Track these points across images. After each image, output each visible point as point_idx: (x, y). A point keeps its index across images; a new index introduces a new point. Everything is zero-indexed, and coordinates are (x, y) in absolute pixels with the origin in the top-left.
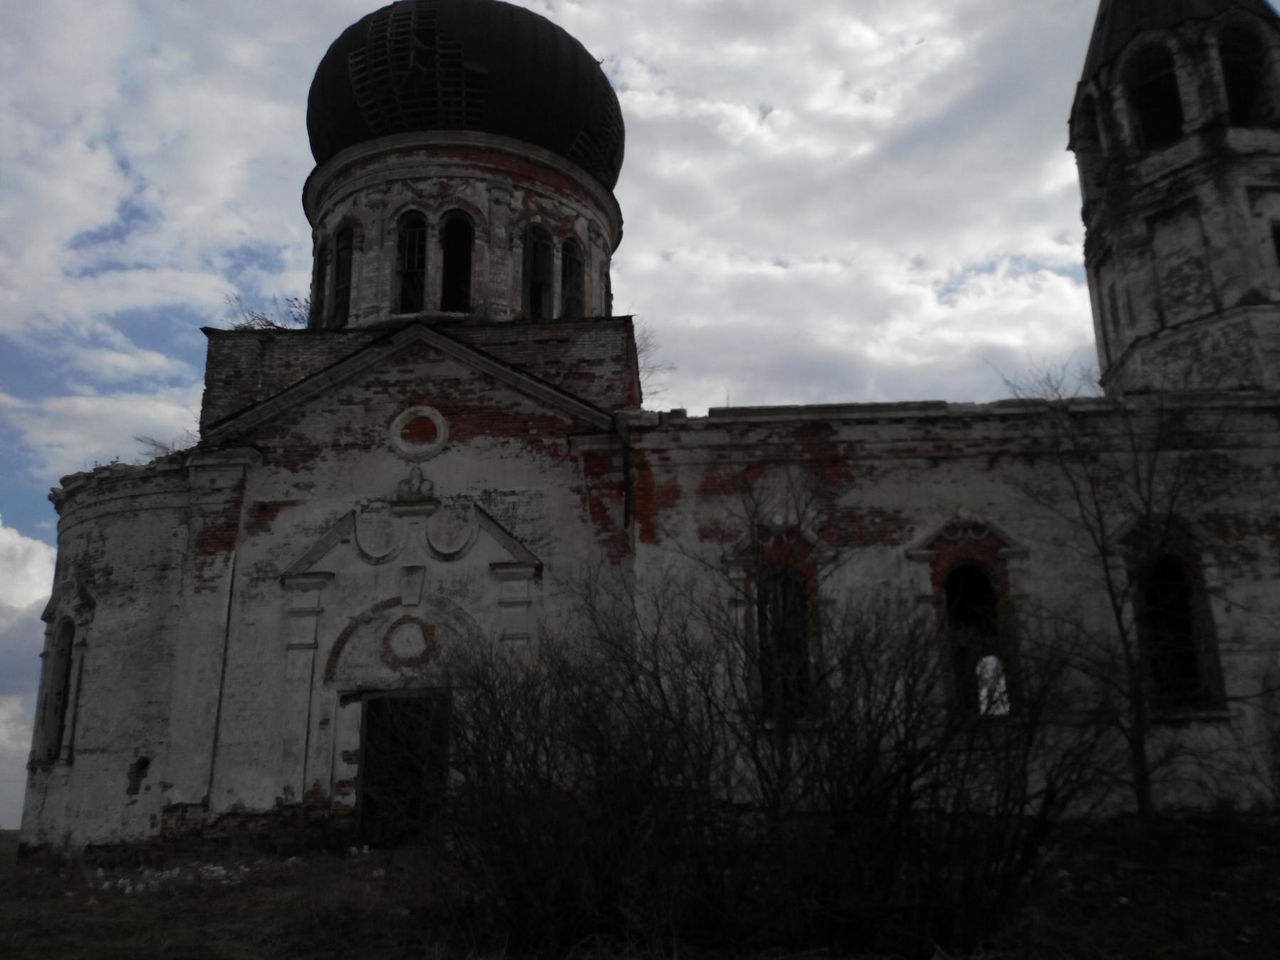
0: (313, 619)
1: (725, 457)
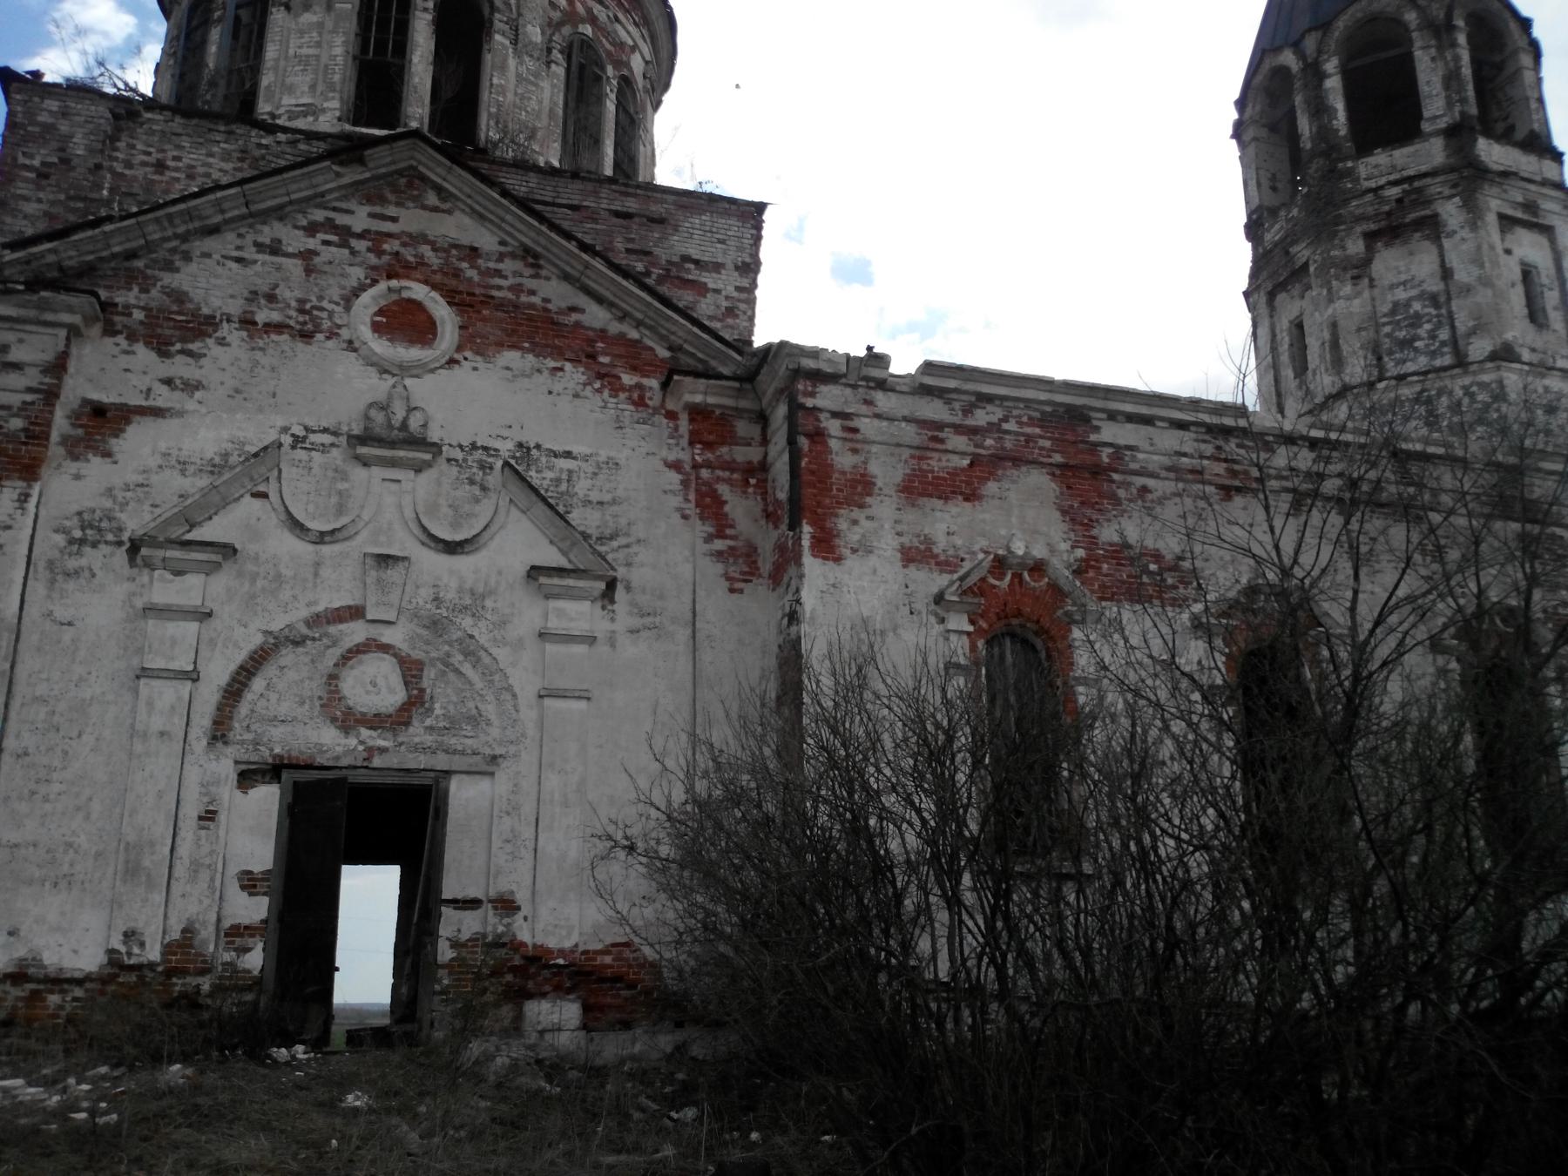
0: (193, 626)
1: (942, 441)
